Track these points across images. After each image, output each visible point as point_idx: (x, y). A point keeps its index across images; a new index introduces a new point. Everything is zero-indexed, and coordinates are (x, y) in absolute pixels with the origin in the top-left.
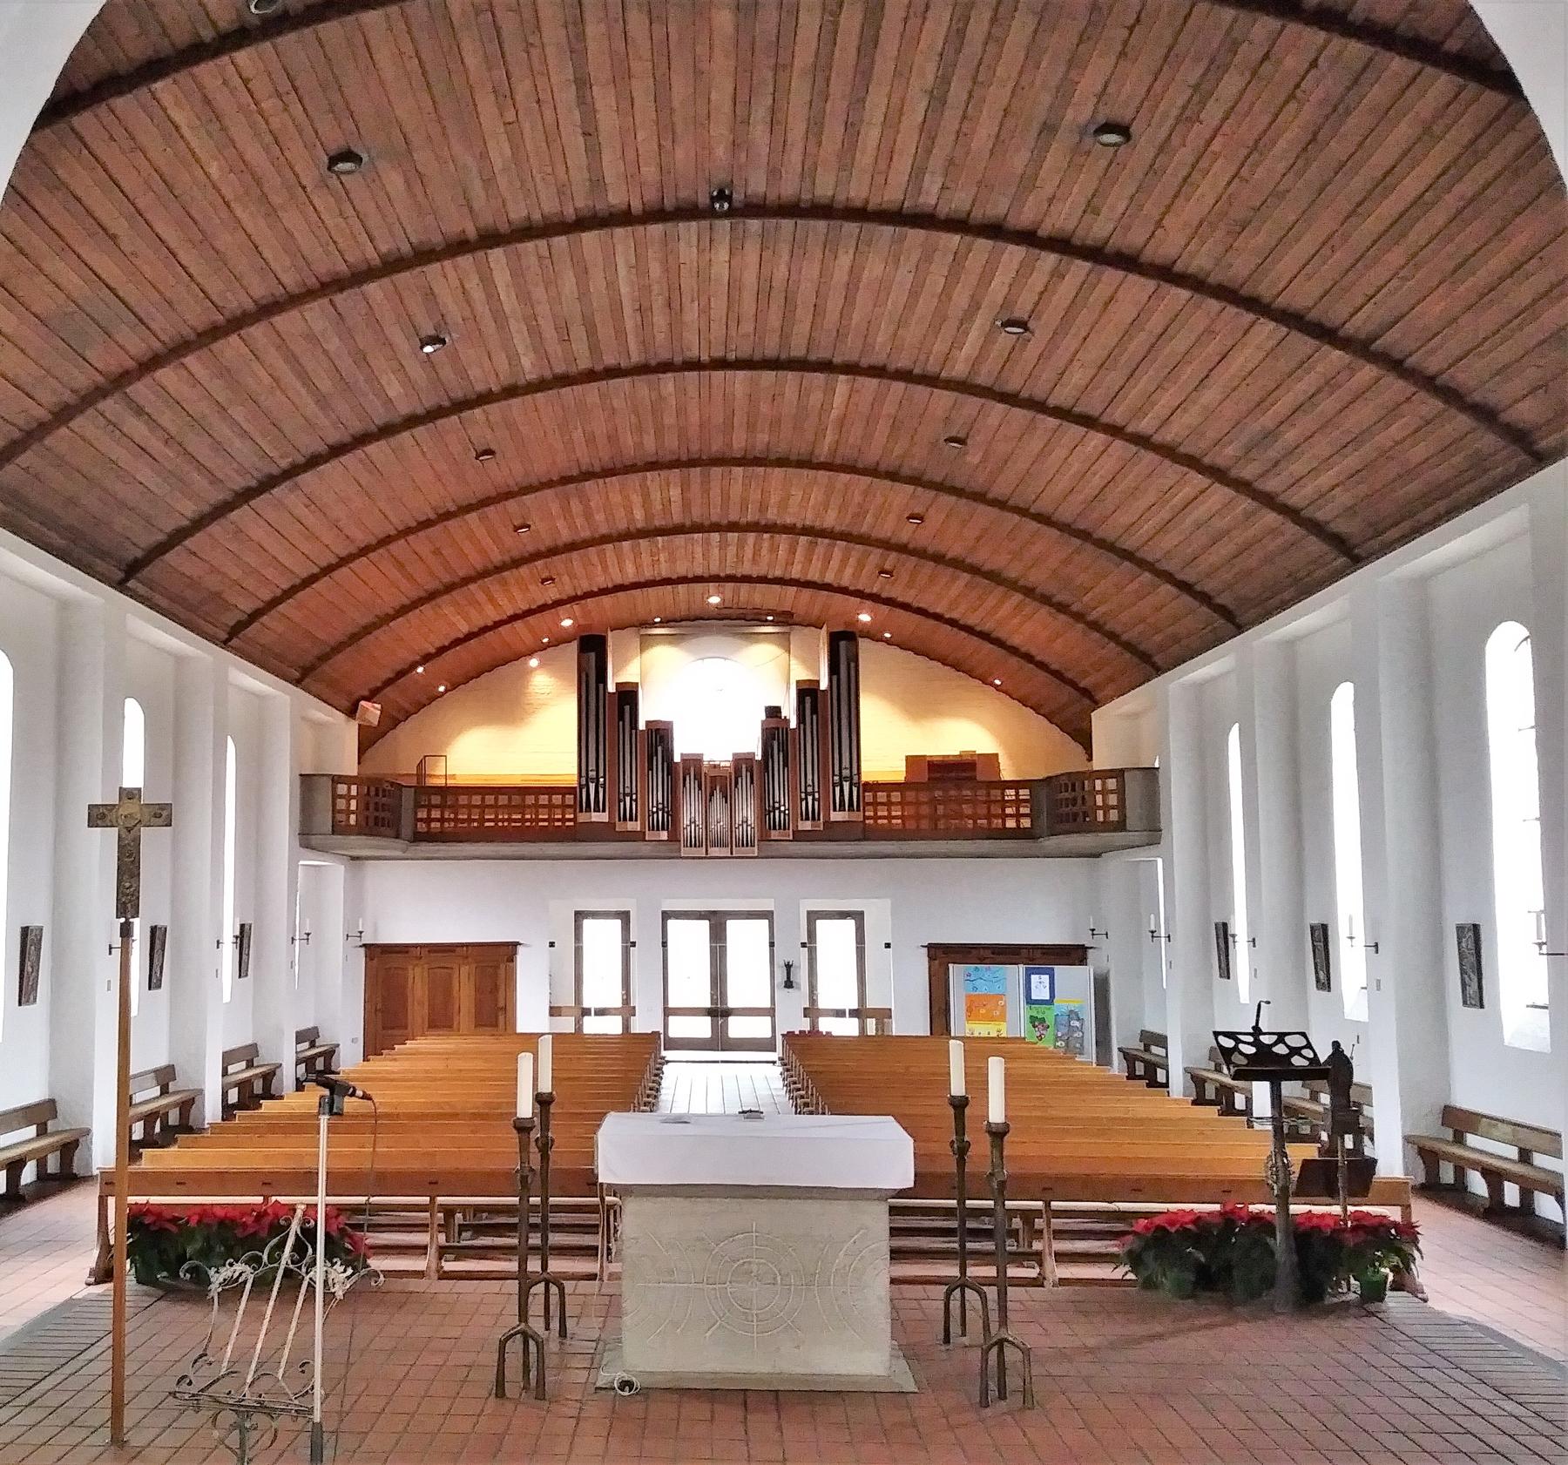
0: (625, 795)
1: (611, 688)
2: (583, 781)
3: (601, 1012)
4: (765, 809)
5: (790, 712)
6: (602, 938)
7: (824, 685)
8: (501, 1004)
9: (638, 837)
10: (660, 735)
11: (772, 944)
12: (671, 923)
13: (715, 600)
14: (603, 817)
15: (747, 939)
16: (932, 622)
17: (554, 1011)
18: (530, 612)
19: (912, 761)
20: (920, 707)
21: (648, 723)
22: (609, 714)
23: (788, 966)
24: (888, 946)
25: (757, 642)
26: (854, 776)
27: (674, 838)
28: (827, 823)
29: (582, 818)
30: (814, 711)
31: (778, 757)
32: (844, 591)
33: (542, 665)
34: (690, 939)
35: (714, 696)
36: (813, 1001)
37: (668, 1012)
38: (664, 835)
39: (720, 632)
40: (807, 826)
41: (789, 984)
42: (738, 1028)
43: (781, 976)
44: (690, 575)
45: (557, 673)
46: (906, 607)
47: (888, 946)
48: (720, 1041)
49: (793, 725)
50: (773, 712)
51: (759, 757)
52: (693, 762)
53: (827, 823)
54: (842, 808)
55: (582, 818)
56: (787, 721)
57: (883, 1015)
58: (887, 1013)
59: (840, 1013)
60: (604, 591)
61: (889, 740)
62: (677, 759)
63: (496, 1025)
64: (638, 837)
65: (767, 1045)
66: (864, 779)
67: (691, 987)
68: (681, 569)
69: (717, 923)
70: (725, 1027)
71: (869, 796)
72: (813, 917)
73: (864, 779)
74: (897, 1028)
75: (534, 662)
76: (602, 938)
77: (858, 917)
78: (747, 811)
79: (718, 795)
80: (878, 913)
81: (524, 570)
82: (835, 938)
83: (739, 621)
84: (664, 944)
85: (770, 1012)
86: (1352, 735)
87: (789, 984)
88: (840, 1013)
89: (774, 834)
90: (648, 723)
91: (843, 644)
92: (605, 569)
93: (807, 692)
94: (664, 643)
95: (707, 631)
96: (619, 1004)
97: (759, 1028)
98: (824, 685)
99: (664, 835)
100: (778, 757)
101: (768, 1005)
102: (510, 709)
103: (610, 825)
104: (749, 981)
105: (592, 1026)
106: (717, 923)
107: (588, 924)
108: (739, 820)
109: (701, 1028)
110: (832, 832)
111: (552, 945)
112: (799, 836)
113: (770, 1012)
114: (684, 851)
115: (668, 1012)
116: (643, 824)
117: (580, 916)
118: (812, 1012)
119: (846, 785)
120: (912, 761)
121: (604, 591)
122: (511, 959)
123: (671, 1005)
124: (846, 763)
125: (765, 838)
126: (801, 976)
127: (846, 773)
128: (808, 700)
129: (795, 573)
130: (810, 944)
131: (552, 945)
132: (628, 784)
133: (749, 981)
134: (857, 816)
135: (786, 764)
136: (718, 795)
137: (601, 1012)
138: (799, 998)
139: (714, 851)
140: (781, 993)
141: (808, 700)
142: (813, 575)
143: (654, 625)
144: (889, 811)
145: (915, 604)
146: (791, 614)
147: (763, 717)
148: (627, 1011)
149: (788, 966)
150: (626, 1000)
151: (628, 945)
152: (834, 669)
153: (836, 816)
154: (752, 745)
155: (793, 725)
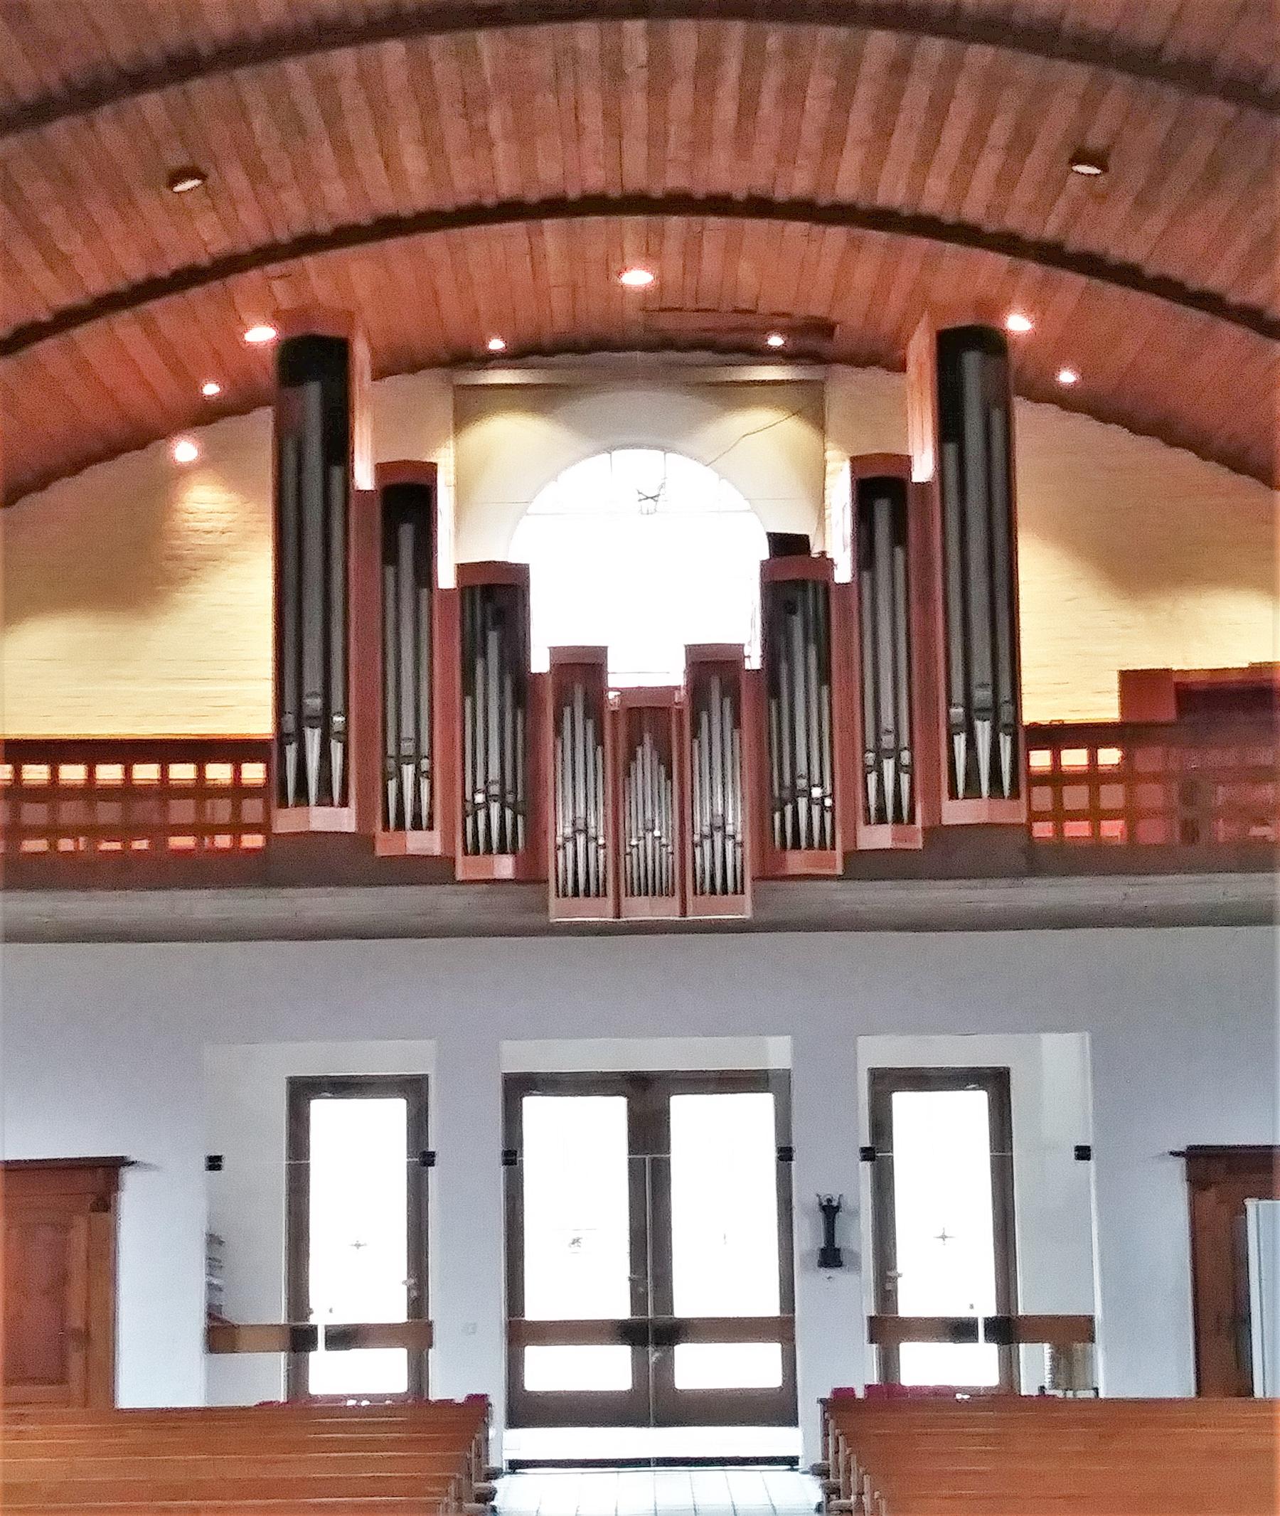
0: (400, 760)
1: (364, 478)
2: (290, 723)
3: (344, 1338)
4: (771, 798)
5: (836, 543)
6: (359, 1147)
7: (923, 469)
8: (76, 1322)
9: (436, 871)
10: (498, 595)
11: (785, 1154)
12: (532, 1105)
13: (637, 278)
14: (343, 820)
15: (723, 1145)
16: (1197, 317)
17: (221, 1335)
18: (152, 289)
19: (1135, 684)
20: (1139, 563)
21: (462, 569)
22: (359, 550)
23: (830, 1211)
24: (1083, 1153)
25: (744, 404)
26: (795, 1039)
27: (532, 873)
28: (935, 832)
29: (287, 821)
30: (899, 536)
31: (804, 660)
32: (968, 234)
33: (212, 460)
34: (576, 1145)
35: (638, 538)
36: (886, 1291)
37: (520, 1333)
38: (505, 866)
39: (652, 377)
40: (879, 837)
41: (831, 1257)
42: (696, 1368)
43: (807, 1238)
44: (573, 194)
45: (235, 480)
46: (1129, 276)
47: (1083, 1153)
48: (654, 1403)
49: (843, 573)
50: (787, 547)
51: (754, 661)
52: (583, 667)
53: (935, 832)
54: (973, 790)
55: (287, 821)
56: (826, 563)
57: (1070, 1334)
58: (1082, 1328)
59: (960, 1330)
60: (346, 236)
61: (1076, 648)
62: (540, 663)
63: (62, 1379)
64: (436, 871)
65: (774, 1408)
66: (1028, 717)
67: (579, 1269)
68: (551, 175)
69: (647, 1104)
70: (666, 1366)
71: (1040, 760)
72: (887, 1082)
73: (1028, 717)
74: (1109, 1375)
75: (185, 450)
76: (359, 1147)
77: (996, 1082)
78: (726, 806)
79: (646, 753)
80: (1056, 1074)
81: (109, 128)
82: (940, 1140)
83: (692, 353)
84: (512, 1157)
85: (779, 1329)
86: (627, 1233)
87: (831, 1257)
88: (960, 1330)
89: (796, 862)
90: (462, 569)
91: (972, 361)
92: (348, 171)
93: (879, 488)
94: (512, 407)
95: (628, 377)
96: (398, 1313)
97: (756, 1367)
98: (923, 469)
99: (505, 866)
100: (804, 660)
101: (770, 1308)
102: (134, 575)
103: (361, 841)
104: (728, 1253)
105: (332, 1374)
106: (647, 1104)
107: (322, 1110)
108: (702, 823)
109: (611, 1368)
110: (947, 853)
111: (214, 1163)
112: (862, 865)
113: (779, 1329)
114: (560, 910)
115: (520, 1333)
116: (448, 840)
117: (302, 1091)
118: (887, 1329)
119: (983, 730)
120: (1135, 684)
121: (346, 236)
122: (105, 1202)
123: (534, 1311)
124: (981, 672)
125: (769, 872)
126: (859, 1235)
127: (982, 696)
128: (882, 510)
129: (847, 187)
130: (877, 1153)
131: (214, 1163)
132: (408, 730)
133: (728, 1253)
134: (1010, 812)
135: (825, 676)
136: (646, 753)
137: (344, 1338)
138: (853, 1292)
139: (641, 909)
140: (808, 1282)
141: (882, 510)
142: (892, 192)
143: (489, 360)
144: (1094, 796)
145: (1151, 270)
146: (825, 328)
147: (766, 555)
148: (416, 1334)
149: (830, 1211)
150: (418, 1304)
151: (422, 1159)
152: (949, 429)
153: (957, 812)
154: (739, 625)
155: (843, 573)
